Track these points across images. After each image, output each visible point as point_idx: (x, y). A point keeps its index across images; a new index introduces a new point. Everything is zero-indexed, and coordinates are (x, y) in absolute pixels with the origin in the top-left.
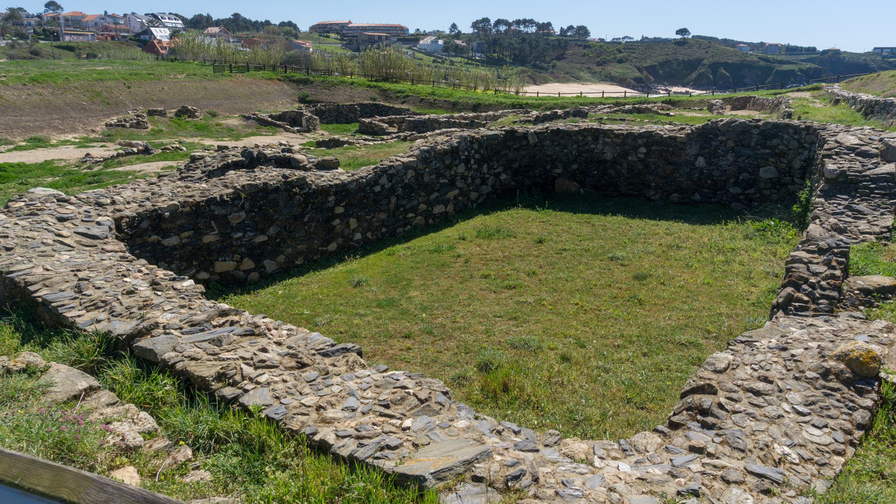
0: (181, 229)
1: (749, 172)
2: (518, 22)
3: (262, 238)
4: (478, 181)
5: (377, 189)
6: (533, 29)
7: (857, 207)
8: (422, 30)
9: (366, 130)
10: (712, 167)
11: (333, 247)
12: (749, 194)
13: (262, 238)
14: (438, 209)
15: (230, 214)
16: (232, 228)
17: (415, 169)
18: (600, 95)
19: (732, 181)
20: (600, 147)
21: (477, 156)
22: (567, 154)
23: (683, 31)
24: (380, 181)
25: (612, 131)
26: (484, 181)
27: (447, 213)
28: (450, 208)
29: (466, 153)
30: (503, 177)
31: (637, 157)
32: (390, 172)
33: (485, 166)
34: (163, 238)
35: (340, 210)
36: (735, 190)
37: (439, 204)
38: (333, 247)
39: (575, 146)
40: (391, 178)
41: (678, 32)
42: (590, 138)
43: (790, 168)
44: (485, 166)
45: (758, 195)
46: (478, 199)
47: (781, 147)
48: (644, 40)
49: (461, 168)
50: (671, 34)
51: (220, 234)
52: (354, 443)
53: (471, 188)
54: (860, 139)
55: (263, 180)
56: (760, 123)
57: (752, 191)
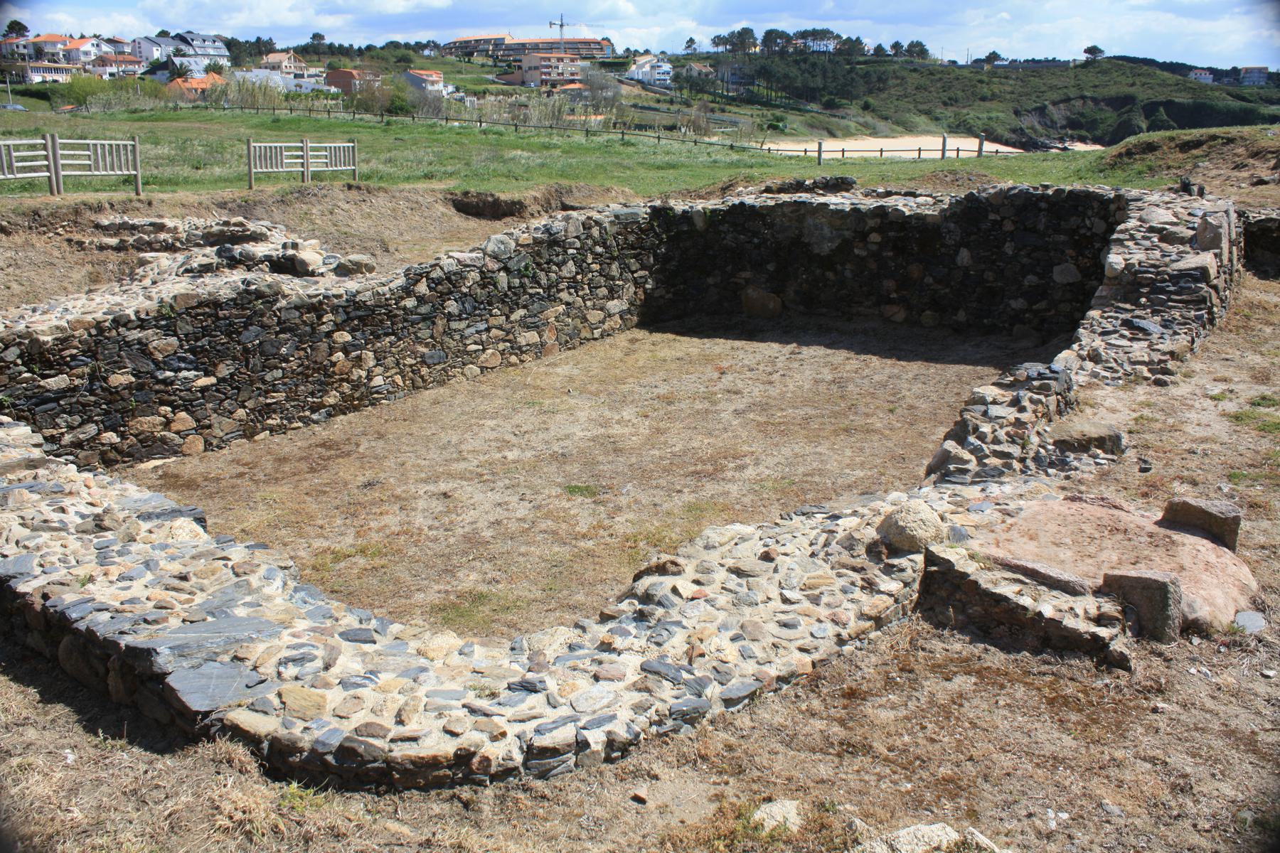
2: (804, 35)
3: (204, 381)
4: (603, 291)
6: (831, 46)
7: (1143, 323)
8: (632, 49)
10: (983, 266)
11: (332, 399)
13: (204, 381)
18: (915, 155)
22: (758, 247)
23: (1092, 50)
25: (826, 205)
36: (1018, 304)
38: (332, 399)
40: (434, 283)
41: (1088, 51)
45: (1053, 312)
46: (603, 322)
54: (1175, 215)
55: (208, 288)
56: (1050, 192)
57: (1042, 305)
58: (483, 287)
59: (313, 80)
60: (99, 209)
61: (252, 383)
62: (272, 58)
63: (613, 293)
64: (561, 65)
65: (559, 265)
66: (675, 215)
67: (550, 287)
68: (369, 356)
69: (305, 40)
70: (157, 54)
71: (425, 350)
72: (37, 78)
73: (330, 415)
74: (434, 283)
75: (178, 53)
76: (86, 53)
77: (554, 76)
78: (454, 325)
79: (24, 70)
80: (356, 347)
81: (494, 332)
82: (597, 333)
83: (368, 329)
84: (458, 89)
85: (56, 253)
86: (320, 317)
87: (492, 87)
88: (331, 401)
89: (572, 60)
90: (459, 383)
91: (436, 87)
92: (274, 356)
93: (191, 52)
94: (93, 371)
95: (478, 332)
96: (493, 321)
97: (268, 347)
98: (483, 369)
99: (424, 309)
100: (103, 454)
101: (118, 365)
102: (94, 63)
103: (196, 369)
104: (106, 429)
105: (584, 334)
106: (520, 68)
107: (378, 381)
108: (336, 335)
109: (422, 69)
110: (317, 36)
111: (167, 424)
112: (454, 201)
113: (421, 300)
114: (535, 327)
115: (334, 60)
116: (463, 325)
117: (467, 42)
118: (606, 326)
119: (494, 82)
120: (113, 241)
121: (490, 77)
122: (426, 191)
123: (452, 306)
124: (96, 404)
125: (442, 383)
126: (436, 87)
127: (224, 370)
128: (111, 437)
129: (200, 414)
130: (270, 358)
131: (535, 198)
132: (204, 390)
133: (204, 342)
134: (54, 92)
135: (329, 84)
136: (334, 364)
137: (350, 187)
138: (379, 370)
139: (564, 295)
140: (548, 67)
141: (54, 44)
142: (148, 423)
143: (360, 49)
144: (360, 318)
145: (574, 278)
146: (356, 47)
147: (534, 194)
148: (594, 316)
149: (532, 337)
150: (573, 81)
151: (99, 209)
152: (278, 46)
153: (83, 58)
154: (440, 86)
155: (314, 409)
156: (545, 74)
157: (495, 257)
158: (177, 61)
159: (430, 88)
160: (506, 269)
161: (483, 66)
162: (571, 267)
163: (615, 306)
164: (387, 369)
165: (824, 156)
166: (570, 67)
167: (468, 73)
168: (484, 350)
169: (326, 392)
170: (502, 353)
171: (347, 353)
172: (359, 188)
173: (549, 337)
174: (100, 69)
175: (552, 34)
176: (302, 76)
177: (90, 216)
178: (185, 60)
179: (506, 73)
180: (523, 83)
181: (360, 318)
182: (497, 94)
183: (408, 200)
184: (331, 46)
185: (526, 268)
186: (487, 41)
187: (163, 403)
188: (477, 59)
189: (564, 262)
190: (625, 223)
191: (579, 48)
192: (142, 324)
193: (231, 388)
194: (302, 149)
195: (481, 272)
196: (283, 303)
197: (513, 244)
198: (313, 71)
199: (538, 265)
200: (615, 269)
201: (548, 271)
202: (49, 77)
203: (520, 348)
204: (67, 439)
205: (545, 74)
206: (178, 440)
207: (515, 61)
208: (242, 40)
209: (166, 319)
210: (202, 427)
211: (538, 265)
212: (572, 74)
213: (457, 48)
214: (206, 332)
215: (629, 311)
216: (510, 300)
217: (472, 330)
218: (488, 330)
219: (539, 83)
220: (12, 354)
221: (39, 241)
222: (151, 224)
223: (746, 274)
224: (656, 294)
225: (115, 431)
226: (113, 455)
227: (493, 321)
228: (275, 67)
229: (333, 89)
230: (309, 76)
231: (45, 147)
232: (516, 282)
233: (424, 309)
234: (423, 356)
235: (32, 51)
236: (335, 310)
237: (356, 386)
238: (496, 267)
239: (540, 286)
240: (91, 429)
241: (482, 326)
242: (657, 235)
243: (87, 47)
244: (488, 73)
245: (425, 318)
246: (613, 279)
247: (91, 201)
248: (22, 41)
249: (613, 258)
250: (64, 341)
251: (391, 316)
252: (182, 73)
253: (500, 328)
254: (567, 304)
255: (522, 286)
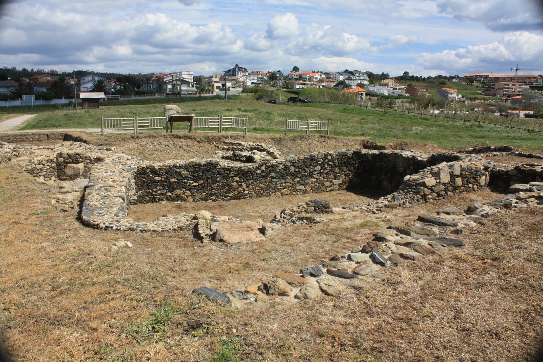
11: (231, 195)
38: (231, 195)
40: (267, 167)
46: (331, 186)
58: (285, 170)
59: (400, 91)
60: (227, 137)
61: (208, 187)
62: (386, 81)
63: (335, 177)
64: (514, 88)
65: (314, 166)
66: (361, 155)
67: (310, 173)
68: (244, 185)
69: (401, 74)
70: (341, 78)
71: (263, 186)
72: (297, 87)
73: (230, 199)
74: (267, 167)
75: (349, 79)
76: (316, 78)
77: (510, 92)
78: (273, 180)
79: (293, 84)
80: (241, 182)
81: (287, 184)
82: (328, 189)
83: (244, 178)
84: (463, 97)
85: (211, 149)
86: (230, 172)
87: (479, 96)
88: (231, 195)
89: (520, 85)
90: (273, 197)
91: (453, 96)
92: (215, 180)
93: (354, 78)
94: (167, 177)
95: (282, 183)
96: (287, 181)
97: (213, 178)
98: (282, 194)
99: (263, 174)
100: (167, 197)
101: (173, 177)
102: (318, 82)
104: (169, 192)
105: (323, 189)
106: (494, 88)
107: (246, 192)
108: (235, 178)
109: (449, 88)
110: (406, 73)
111: (184, 193)
112: (363, 144)
113: (263, 171)
114: (303, 184)
115: (412, 83)
116: (276, 180)
117: (471, 76)
118: (332, 188)
119: (481, 94)
120: (226, 147)
121: (480, 92)
122: (353, 140)
123: (273, 174)
124: (167, 185)
125: (267, 196)
126: (453, 96)
127: (201, 182)
128: (169, 194)
129: (192, 192)
130: (214, 181)
131: (391, 146)
132: (194, 186)
133: (196, 174)
134: (301, 92)
135: (406, 93)
136: (233, 185)
137: (321, 137)
138: (247, 189)
139: (316, 176)
140: (507, 88)
141: (306, 75)
142: (178, 192)
143: (424, 78)
144: (242, 174)
146: (423, 77)
147: (390, 144)
148: (327, 184)
149: (302, 187)
150: (519, 95)
151: (227, 137)
152: (390, 76)
153: (315, 80)
154: (455, 95)
155: (226, 197)
156: (506, 91)
157: (290, 162)
158: (347, 82)
159: (450, 96)
160: (293, 165)
161: (477, 87)
162: (319, 167)
163: (336, 181)
164: (250, 189)
166: (517, 88)
167: (470, 90)
168: (283, 189)
169: (230, 193)
170: (290, 190)
171: (237, 183)
172: (325, 137)
173: (308, 188)
174: (319, 84)
175: (512, 74)
176: (396, 89)
177: (224, 139)
178: (350, 81)
179: (487, 90)
180: (495, 95)
181: (242, 174)
182: (481, 100)
183: (343, 142)
184: (412, 77)
185: (301, 166)
186: (481, 76)
187: (183, 188)
188: (475, 84)
189: (316, 166)
190: (342, 156)
191: (523, 80)
192: (180, 167)
193: (202, 188)
194: (307, 123)
195: (284, 166)
196: (219, 167)
197: (297, 159)
198: (401, 87)
199: (306, 165)
200: (337, 170)
201: (310, 168)
202: (301, 87)
203: (297, 190)
204: (159, 192)
205: (506, 91)
206: (186, 198)
207: (493, 85)
208: (375, 74)
209: (186, 167)
211: (306, 165)
212: (519, 92)
213: (467, 79)
214: (197, 172)
215: (342, 184)
216: (294, 175)
217: (280, 182)
218: (286, 183)
219: (502, 95)
220: (148, 170)
221: (207, 145)
222: (238, 143)
223: (383, 177)
224: (354, 180)
226: (169, 198)
227: (287, 181)
228: (386, 85)
229: (407, 95)
230: (399, 89)
231: (218, 119)
232: (297, 170)
233: (263, 174)
234: (262, 187)
235: (298, 77)
236: (235, 171)
237: (239, 192)
238: (290, 164)
240: (165, 191)
241: (283, 182)
242: (355, 160)
243: (317, 76)
244: (479, 90)
245: (263, 177)
246: (336, 173)
247: (210, 135)
248: (296, 74)
249: (336, 167)
250: (161, 169)
251: (252, 175)
252: (347, 86)
253: (290, 183)
254: (317, 179)
255: (299, 171)
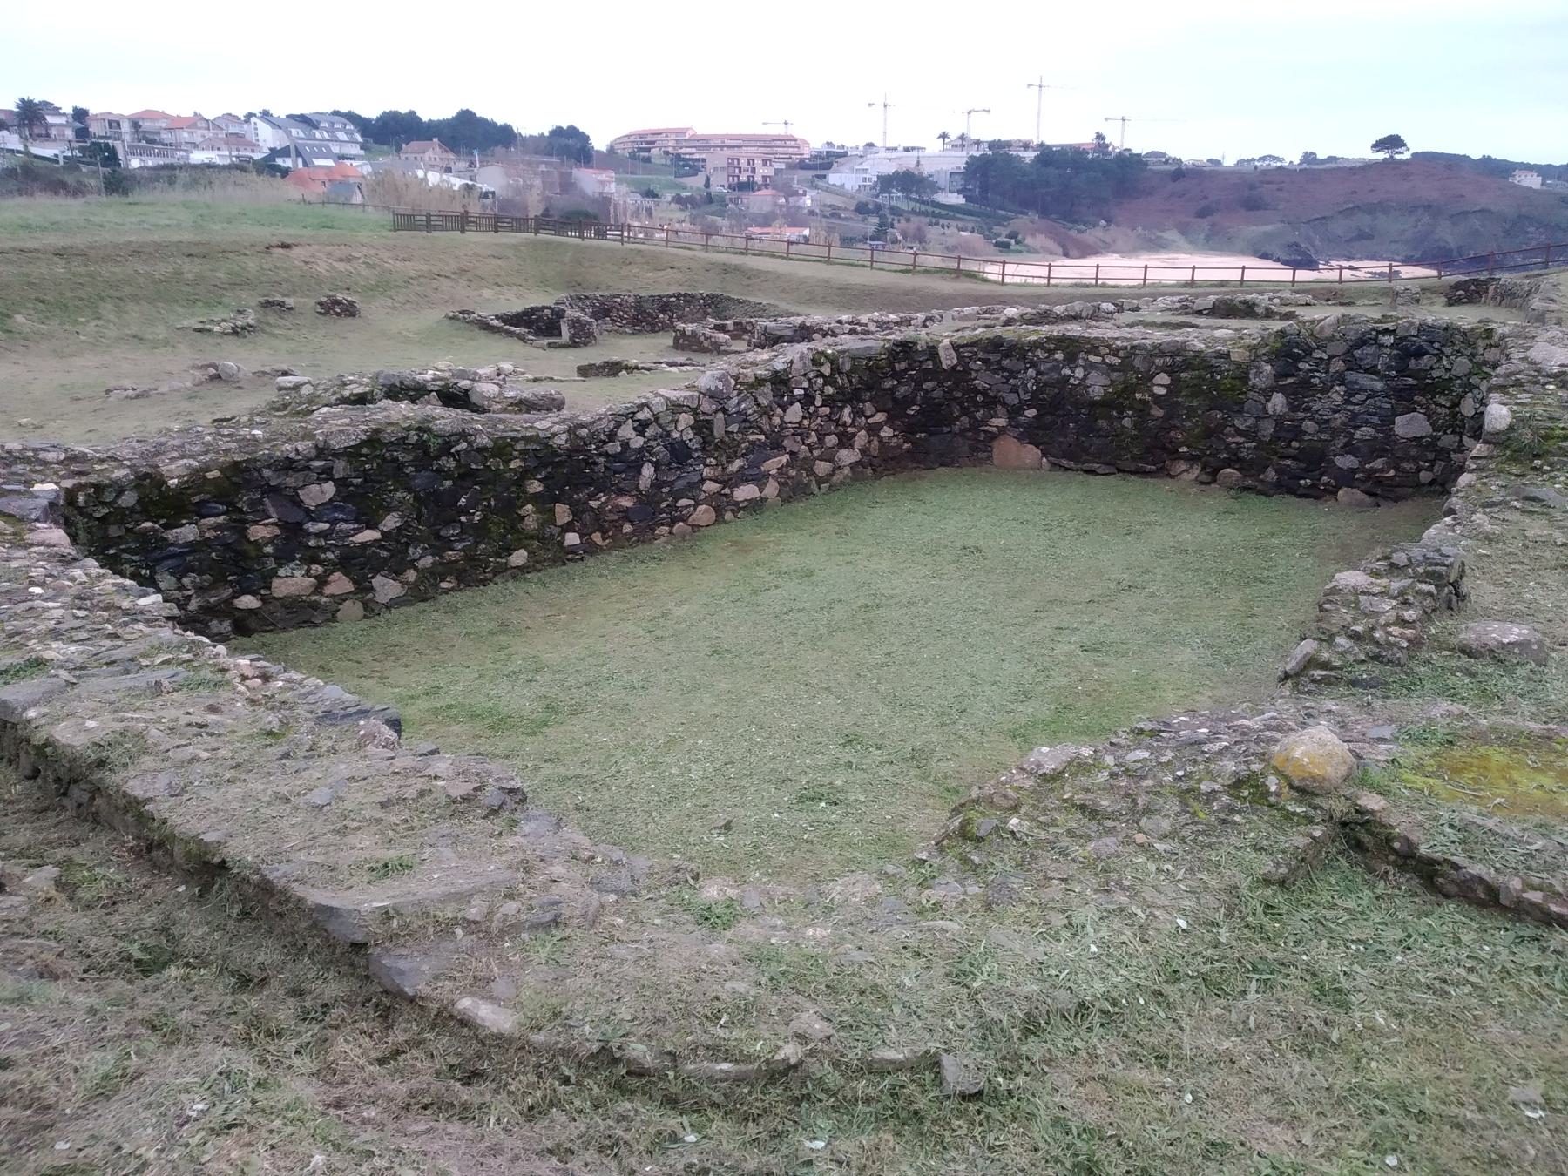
0: (201, 511)
1: (1374, 426)
3: (369, 535)
4: (831, 440)
5: (614, 448)
9: (687, 343)
12: (1374, 471)
13: (369, 535)
14: (745, 492)
15: (302, 487)
16: (308, 511)
17: (695, 412)
19: (1341, 442)
20: (1079, 373)
21: (830, 390)
23: (1392, 142)
24: (620, 433)
26: (846, 440)
27: (764, 500)
28: (771, 489)
29: (806, 385)
30: (886, 432)
31: (1153, 395)
32: (640, 416)
33: (847, 411)
34: (167, 527)
35: (535, 487)
36: (1346, 462)
37: (747, 481)
39: (1031, 372)
41: (1380, 145)
42: (1059, 356)
43: (1454, 416)
44: (847, 411)
47: (1435, 374)
48: (1487, 161)
49: (795, 413)
50: (1358, 149)
51: (283, 525)
52: (132, 788)
53: (816, 453)
103: (356, 521)
145: (800, 423)
165: (1007, 280)
210: (363, 588)
225: (254, 593)
239: (762, 432)
